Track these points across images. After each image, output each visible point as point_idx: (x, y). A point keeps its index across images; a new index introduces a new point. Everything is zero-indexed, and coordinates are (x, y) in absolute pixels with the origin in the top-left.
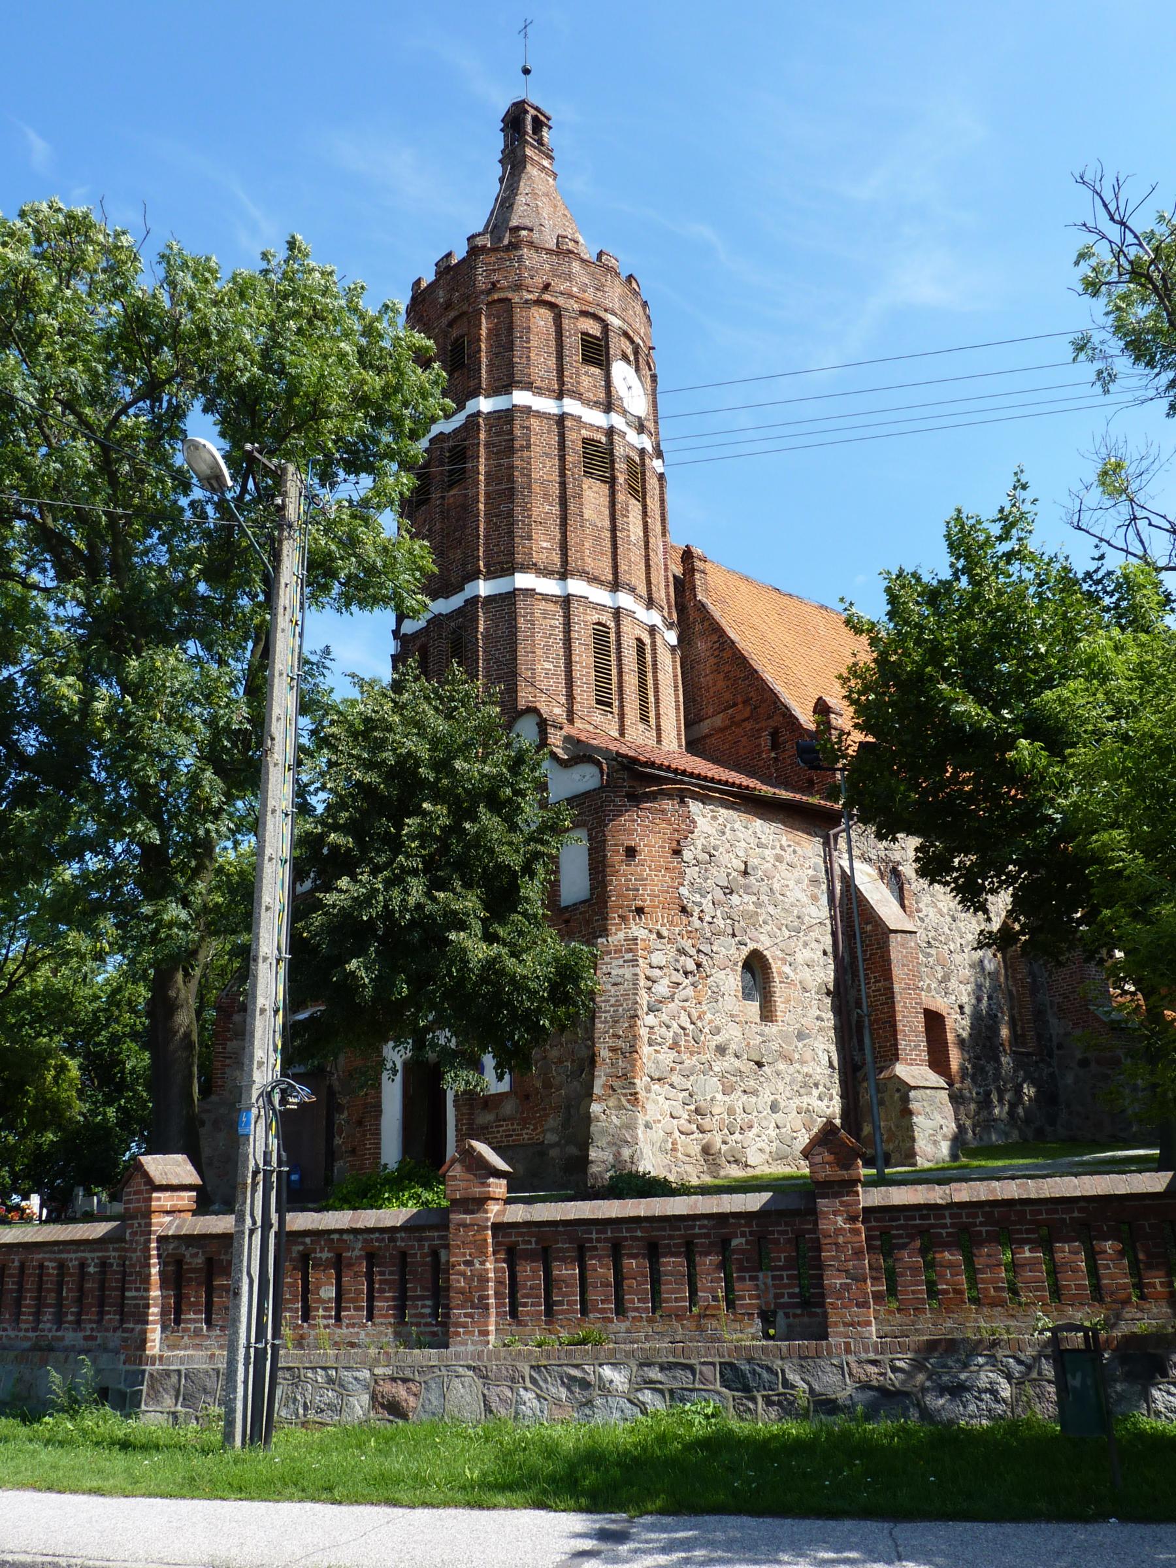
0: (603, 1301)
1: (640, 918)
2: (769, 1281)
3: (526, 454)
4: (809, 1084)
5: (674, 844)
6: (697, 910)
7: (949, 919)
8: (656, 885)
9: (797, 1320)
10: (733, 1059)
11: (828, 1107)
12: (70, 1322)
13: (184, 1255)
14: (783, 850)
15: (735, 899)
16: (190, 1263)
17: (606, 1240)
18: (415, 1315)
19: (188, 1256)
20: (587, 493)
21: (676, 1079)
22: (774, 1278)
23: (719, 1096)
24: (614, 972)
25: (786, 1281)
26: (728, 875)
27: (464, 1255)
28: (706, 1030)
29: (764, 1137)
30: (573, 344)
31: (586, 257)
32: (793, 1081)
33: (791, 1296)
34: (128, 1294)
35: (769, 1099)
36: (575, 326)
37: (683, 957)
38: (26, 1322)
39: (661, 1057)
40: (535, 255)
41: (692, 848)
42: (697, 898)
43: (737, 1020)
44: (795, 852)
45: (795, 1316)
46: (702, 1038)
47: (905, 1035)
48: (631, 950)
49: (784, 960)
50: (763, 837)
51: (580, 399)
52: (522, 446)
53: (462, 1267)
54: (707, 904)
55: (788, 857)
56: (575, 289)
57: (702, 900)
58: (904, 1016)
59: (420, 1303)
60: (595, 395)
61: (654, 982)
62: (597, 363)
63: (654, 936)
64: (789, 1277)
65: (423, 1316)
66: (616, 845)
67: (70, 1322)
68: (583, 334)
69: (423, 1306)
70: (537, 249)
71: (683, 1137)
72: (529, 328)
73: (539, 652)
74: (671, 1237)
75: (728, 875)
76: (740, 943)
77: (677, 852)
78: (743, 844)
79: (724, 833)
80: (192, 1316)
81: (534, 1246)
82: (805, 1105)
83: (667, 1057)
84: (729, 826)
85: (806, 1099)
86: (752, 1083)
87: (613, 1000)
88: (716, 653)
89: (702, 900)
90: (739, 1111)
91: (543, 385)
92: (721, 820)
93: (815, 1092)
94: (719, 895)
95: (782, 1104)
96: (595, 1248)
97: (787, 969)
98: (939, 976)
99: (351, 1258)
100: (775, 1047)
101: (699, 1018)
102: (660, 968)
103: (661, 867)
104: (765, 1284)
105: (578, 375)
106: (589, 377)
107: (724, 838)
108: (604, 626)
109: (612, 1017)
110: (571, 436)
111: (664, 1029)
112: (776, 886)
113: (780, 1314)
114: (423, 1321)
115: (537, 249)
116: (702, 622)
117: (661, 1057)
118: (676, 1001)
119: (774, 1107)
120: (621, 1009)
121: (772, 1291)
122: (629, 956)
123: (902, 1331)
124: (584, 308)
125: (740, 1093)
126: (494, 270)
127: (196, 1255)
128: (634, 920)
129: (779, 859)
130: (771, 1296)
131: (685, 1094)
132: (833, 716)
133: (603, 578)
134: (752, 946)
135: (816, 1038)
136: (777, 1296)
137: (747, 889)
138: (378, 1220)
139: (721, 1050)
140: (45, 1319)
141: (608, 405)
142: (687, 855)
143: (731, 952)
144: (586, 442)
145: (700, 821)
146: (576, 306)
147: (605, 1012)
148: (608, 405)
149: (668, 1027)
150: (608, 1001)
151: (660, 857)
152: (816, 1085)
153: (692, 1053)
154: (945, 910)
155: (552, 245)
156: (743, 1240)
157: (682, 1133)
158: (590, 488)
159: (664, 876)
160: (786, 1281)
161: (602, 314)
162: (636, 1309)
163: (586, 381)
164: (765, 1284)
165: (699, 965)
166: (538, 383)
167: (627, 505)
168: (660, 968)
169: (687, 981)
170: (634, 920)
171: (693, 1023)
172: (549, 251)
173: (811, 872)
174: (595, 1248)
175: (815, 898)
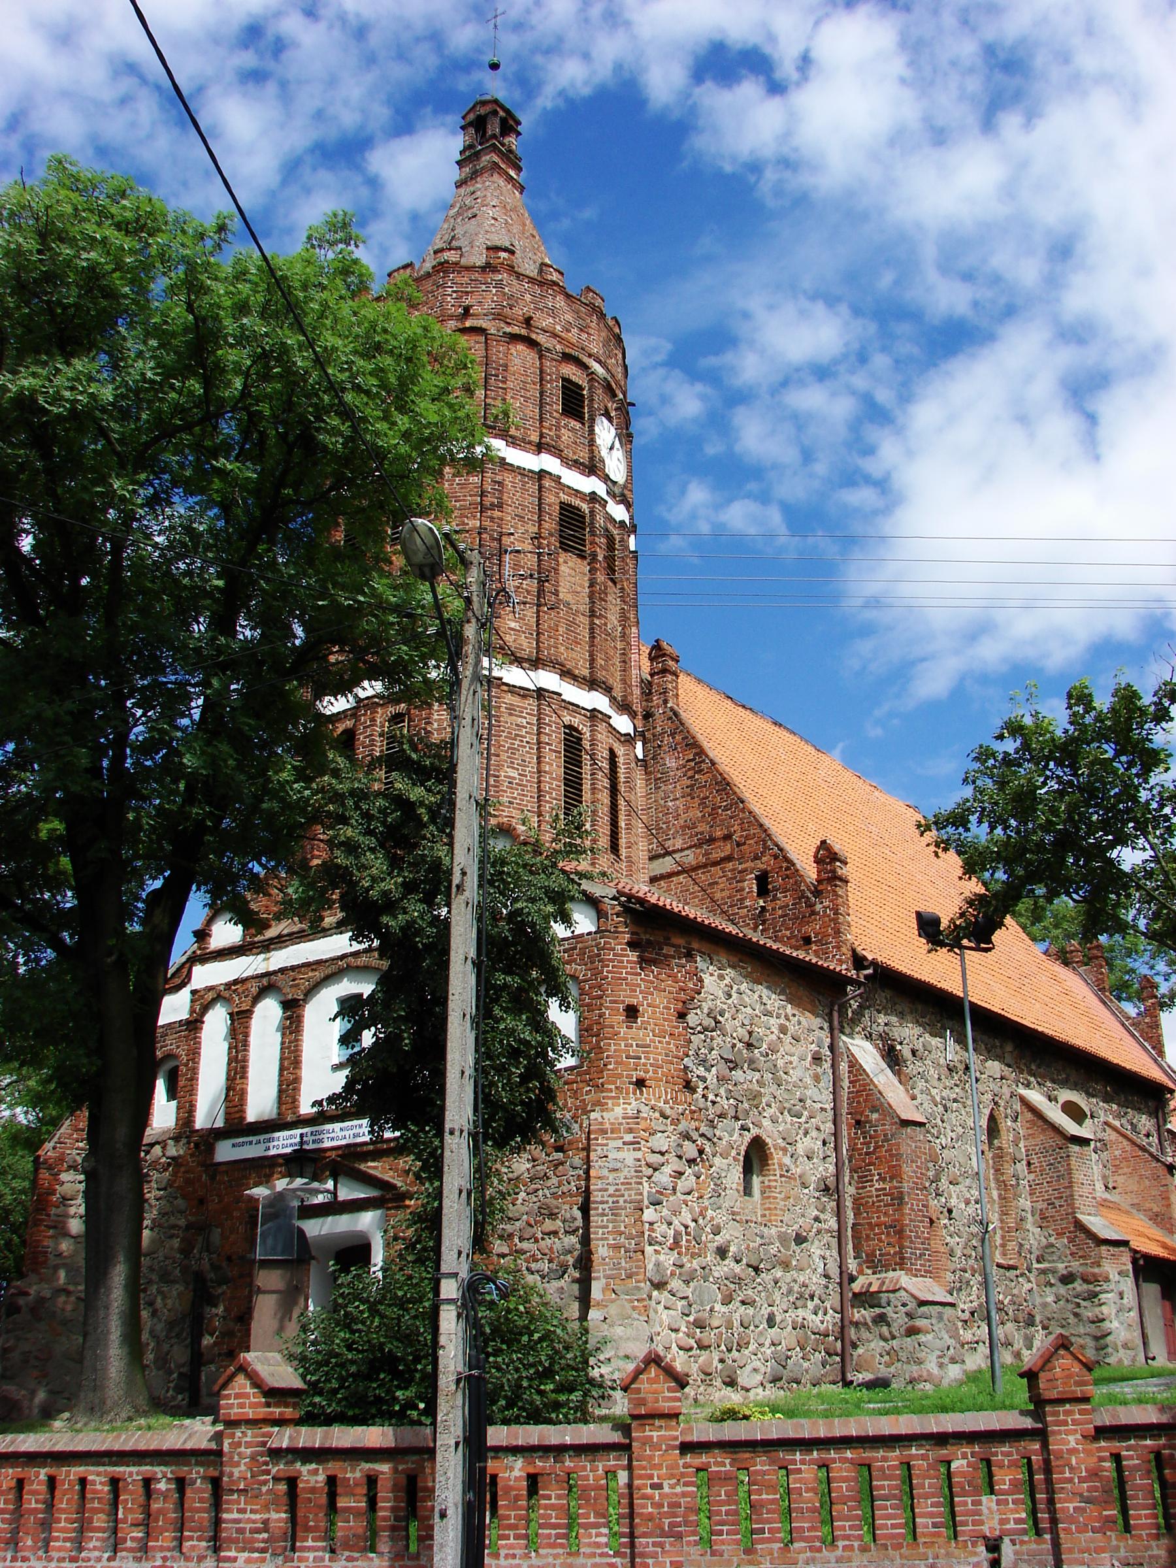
0: (810, 1529)
1: (641, 1093)
2: (994, 1506)
3: (497, 514)
4: (803, 1297)
5: (680, 1006)
6: (701, 1085)
7: (941, 1109)
8: (660, 1054)
9: (1024, 1547)
10: (733, 1264)
11: (822, 1322)
12: (131, 1550)
13: (300, 1472)
14: (788, 1019)
15: (738, 1075)
16: (308, 1482)
17: (811, 1462)
18: (589, 1545)
19: (305, 1473)
20: (563, 568)
21: (675, 1284)
22: (998, 1503)
23: (718, 1307)
24: (611, 1156)
25: (1011, 1505)
26: (734, 1046)
27: (651, 1477)
28: (708, 1229)
29: (760, 1356)
30: (555, 390)
31: (570, 293)
32: (790, 1291)
33: (1018, 1521)
34: (225, 1516)
35: (765, 1311)
36: (558, 370)
37: (686, 1143)
38: (59, 1549)
39: (662, 1258)
40: (515, 282)
41: (698, 1011)
42: (701, 1071)
43: (738, 1218)
44: (799, 1023)
45: (1022, 1542)
46: (704, 1238)
47: (911, 1242)
48: (631, 1131)
49: (785, 1150)
50: (769, 1002)
51: (560, 457)
52: (492, 504)
53: (649, 1491)
54: (711, 1077)
55: (792, 1029)
56: (558, 328)
57: (707, 1075)
58: (911, 1220)
59: (594, 1531)
60: (574, 453)
61: (655, 1170)
62: (579, 417)
63: (657, 1115)
64: (1014, 1502)
65: (598, 1545)
66: (615, 1002)
67: (131, 1550)
68: (564, 379)
69: (597, 1535)
70: (519, 276)
71: (681, 1352)
72: (506, 366)
73: (504, 756)
74: (885, 1459)
75: (734, 1046)
76: (743, 1128)
77: (682, 1016)
78: (749, 1010)
79: (730, 996)
80: (310, 1543)
81: (728, 1468)
82: (800, 1320)
83: (668, 1259)
84: (735, 987)
85: (800, 1312)
86: (750, 1292)
87: (611, 1190)
88: (690, 773)
89: (707, 1075)
90: (736, 1324)
91: (518, 434)
92: (727, 980)
93: (810, 1305)
94: (723, 1068)
95: (778, 1319)
96: (799, 1471)
97: (787, 1160)
98: (931, 1174)
99: (509, 1479)
100: (773, 1250)
101: (701, 1214)
102: (662, 1154)
103: (665, 1031)
104: (989, 1508)
105: (558, 428)
106: (569, 432)
107: (729, 1001)
108: (576, 730)
109: (611, 1209)
110: (550, 499)
111: (665, 1226)
112: (780, 1063)
113: (1006, 1540)
114: (599, 1551)
115: (519, 276)
116: (673, 735)
117: (662, 1258)
118: (678, 1194)
119: (771, 1321)
120: (621, 1200)
121: (997, 1517)
122: (629, 1138)
123: (1135, 1558)
124: (567, 350)
125: (738, 1304)
126: (467, 293)
127: (315, 1472)
128: (634, 1094)
129: (783, 1030)
130: (996, 1521)
131: (684, 1302)
132: (838, 864)
133: (577, 672)
134: (755, 1131)
135: (812, 1243)
136: (1003, 1522)
137: (753, 1065)
138: (541, 1436)
139: (722, 1252)
140: (91, 1545)
141: (592, 467)
142: (692, 1019)
143: (733, 1138)
144: (565, 508)
145: (707, 980)
146: (558, 347)
147: (602, 1202)
148: (592, 467)
149: (670, 1224)
150: (606, 1190)
151: (665, 1020)
152: (812, 1297)
153: (693, 1256)
154: (938, 1099)
155: (531, 270)
156: (964, 1462)
157: (681, 1348)
158: (566, 562)
159: (668, 1043)
160: (1011, 1505)
161: (585, 359)
162: (847, 1537)
163: (566, 436)
164: (989, 1508)
165: (701, 1152)
166: (513, 432)
167: (606, 588)
168: (662, 1154)
169: (690, 1171)
170: (634, 1094)
171: (695, 1221)
172: (532, 280)
173: (814, 1047)
174: (799, 1471)
175: (817, 1078)
